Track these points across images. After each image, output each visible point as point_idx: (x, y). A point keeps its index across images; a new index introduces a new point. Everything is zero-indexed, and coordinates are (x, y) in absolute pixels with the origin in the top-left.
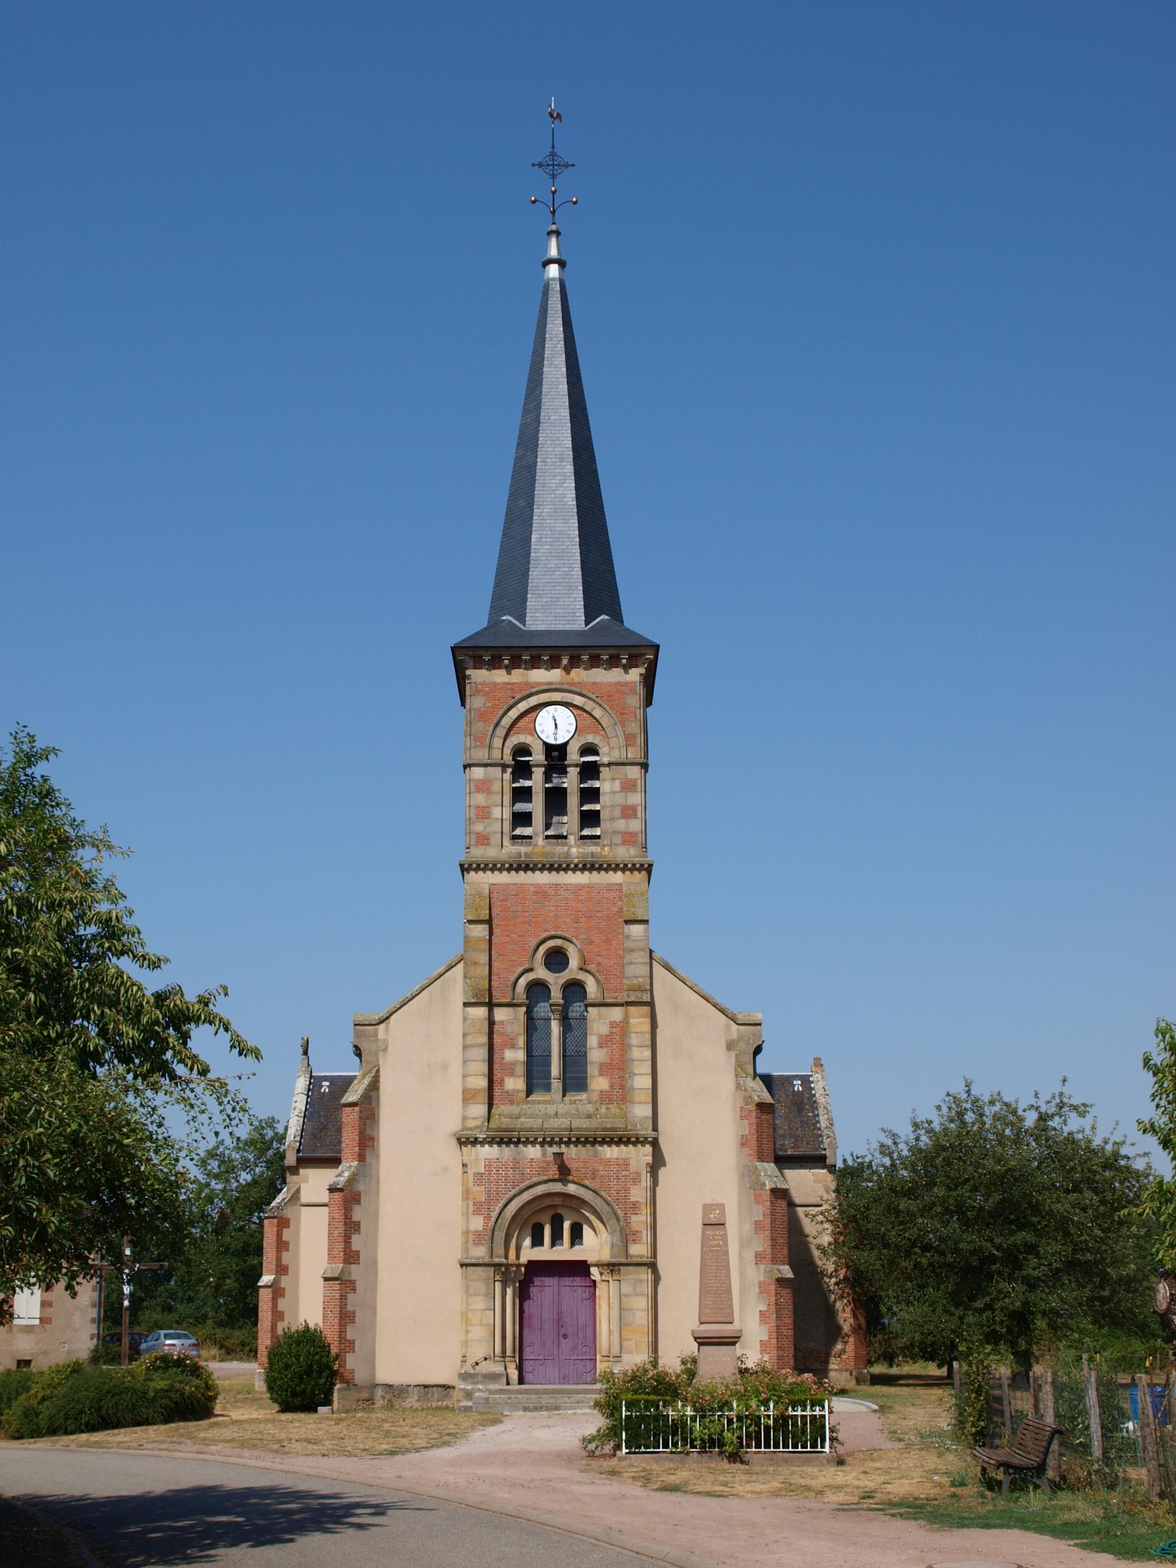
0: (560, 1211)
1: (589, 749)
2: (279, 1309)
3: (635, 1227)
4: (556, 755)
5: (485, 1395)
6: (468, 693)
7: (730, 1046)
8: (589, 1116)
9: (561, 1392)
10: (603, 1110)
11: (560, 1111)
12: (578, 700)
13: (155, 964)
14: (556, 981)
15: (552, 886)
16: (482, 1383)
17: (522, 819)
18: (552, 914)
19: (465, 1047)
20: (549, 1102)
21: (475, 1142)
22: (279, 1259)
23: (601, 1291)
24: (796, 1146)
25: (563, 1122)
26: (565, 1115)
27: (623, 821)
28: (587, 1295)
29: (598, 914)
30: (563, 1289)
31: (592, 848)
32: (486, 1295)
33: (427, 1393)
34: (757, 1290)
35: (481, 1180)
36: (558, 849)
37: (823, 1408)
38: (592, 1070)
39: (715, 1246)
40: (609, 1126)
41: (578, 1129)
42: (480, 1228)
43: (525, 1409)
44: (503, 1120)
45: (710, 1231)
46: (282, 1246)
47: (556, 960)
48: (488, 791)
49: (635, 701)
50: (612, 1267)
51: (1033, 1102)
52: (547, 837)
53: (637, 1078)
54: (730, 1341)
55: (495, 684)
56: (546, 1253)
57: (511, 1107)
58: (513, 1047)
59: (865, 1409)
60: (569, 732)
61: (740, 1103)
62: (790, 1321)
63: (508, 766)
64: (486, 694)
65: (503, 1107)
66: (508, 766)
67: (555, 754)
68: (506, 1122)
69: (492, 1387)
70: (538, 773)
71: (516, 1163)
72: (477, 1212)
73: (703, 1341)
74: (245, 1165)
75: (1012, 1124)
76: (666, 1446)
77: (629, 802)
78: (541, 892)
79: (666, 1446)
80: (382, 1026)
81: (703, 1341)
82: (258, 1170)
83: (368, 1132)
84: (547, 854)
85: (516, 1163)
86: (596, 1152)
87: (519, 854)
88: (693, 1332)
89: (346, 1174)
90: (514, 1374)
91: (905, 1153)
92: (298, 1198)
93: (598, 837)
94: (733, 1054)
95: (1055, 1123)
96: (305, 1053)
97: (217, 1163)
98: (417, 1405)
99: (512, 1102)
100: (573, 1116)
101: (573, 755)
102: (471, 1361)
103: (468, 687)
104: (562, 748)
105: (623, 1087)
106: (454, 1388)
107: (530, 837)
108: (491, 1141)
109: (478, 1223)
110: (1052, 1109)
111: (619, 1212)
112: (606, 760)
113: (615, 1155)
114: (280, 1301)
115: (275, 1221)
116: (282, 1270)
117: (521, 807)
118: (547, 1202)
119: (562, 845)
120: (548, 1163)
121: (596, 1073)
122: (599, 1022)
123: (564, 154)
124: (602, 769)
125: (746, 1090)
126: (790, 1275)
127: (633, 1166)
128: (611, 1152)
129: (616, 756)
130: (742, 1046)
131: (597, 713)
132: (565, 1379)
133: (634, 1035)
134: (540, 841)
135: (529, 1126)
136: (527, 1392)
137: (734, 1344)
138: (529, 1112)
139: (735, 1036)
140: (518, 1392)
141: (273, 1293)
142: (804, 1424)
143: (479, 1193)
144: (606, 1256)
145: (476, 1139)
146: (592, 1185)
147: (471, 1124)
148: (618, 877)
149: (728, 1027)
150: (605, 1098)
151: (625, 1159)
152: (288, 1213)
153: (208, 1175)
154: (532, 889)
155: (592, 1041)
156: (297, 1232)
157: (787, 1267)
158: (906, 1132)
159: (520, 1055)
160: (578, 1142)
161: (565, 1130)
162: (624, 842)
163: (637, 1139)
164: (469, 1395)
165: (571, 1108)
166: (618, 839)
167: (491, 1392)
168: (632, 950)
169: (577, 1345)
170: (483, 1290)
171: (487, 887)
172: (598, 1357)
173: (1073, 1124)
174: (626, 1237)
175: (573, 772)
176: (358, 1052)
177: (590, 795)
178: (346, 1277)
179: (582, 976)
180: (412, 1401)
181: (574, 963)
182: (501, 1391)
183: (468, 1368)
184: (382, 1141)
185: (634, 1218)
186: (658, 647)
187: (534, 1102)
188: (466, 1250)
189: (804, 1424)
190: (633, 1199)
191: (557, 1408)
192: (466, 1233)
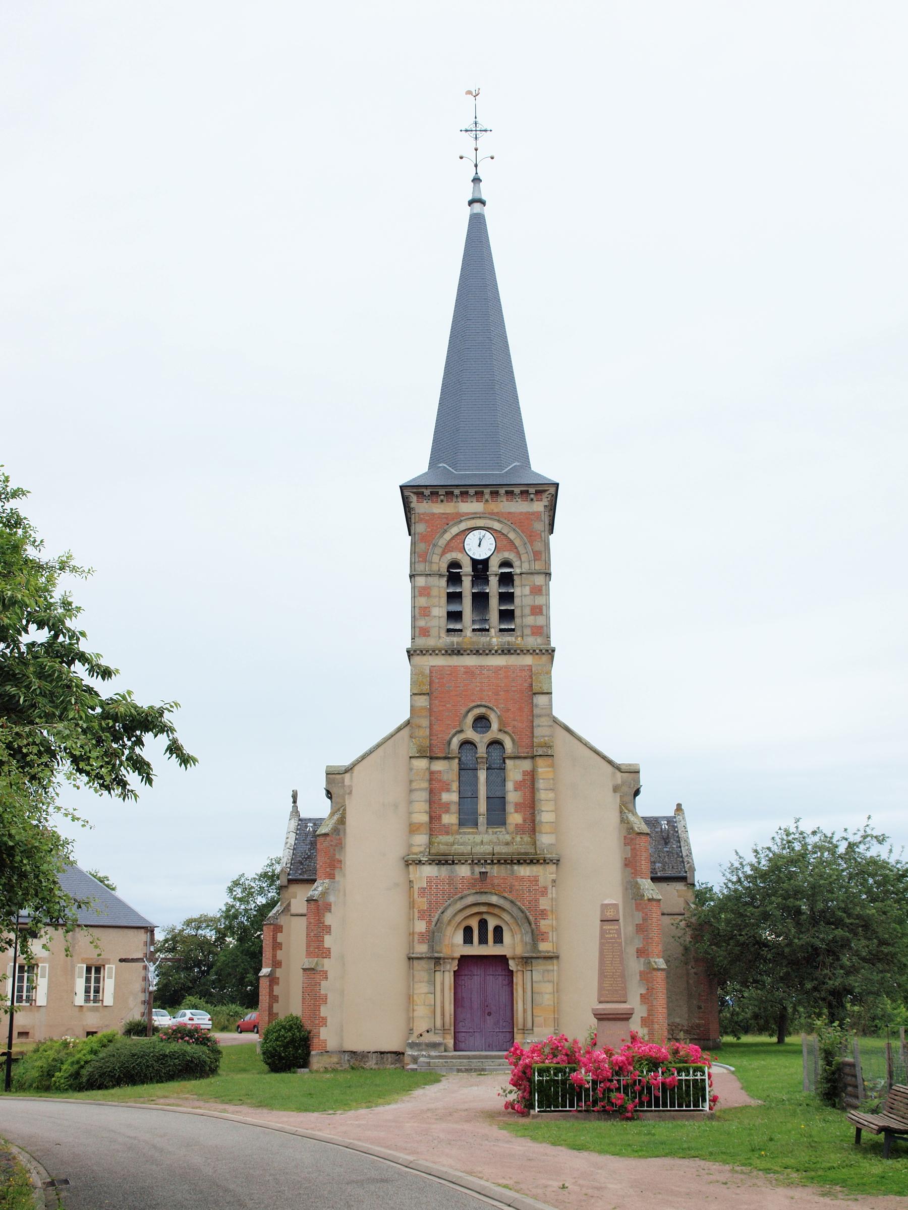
0: (485, 917)
1: (506, 564)
2: (275, 993)
4: (480, 567)
5: (427, 1060)
6: (413, 521)
7: (616, 789)
8: (507, 844)
9: (486, 1057)
10: (518, 839)
11: (485, 840)
12: (497, 526)
13: (106, 673)
14: (481, 740)
15: (477, 667)
17: (455, 616)
18: (478, 689)
19: (411, 791)
20: (476, 833)
22: (274, 956)
23: (518, 979)
24: (664, 869)
25: (487, 849)
27: (532, 617)
28: (505, 982)
29: (513, 689)
30: (488, 977)
31: (508, 638)
32: (429, 982)
33: (382, 1058)
34: (638, 977)
35: (424, 893)
36: (483, 639)
37: (704, 1073)
38: (510, 808)
39: (611, 938)
40: (523, 851)
41: (499, 854)
42: (424, 930)
43: (459, 1071)
44: (441, 847)
45: (607, 927)
46: (277, 946)
47: (482, 722)
48: (428, 595)
49: (539, 526)
50: (526, 961)
51: (844, 835)
52: (474, 630)
53: (544, 814)
54: (625, 1017)
55: (433, 514)
56: (476, 949)
57: (448, 837)
58: (448, 790)
59: (725, 1071)
60: (490, 550)
61: (624, 833)
62: (664, 1001)
63: (443, 576)
64: (427, 521)
66: (443, 576)
67: (480, 566)
68: (443, 848)
70: (467, 581)
71: (451, 880)
72: (421, 918)
73: (602, 1017)
74: (261, 891)
75: (829, 850)
76: (572, 1106)
77: (537, 603)
78: (469, 672)
79: (572, 1106)
80: (347, 776)
81: (602, 1017)
82: (270, 895)
83: (337, 857)
84: (473, 642)
85: (451, 880)
87: (453, 643)
88: (593, 1010)
89: (320, 889)
90: (450, 1042)
91: (750, 872)
92: (289, 910)
93: (513, 630)
94: (618, 795)
95: (861, 848)
96: (295, 802)
97: (240, 890)
98: (374, 1067)
99: (447, 833)
101: (494, 567)
102: (416, 1033)
103: (413, 516)
104: (485, 562)
105: (533, 821)
106: (403, 1054)
107: (461, 631)
108: (431, 862)
109: (421, 926)
110: (857, 839)
111: (531, 918)
112: (518, 571)
113: (528, 874)
114: (275, 987)
115: (272, 927)
116: (276, 964)
117: (454, 608)
119: (485, 636)
120: (475, 880)
121: (513, 810)
122: (515, 771)
123: (483, 124)
124: (515, 577)
125: (628, 823)
126: (664, 966)
127: (542, 882)
128: (524, 871)
129: (526, 567)
130: (625, 789)
131: (512, 536)
132: (490, 1048)
133: (541, 781)
134: (468, 633)
135: (460, 851)
136: (460, 1057)
137: (627, 1019)
138: (461, 841)
139: (619, 782)
140: (453, 1057)
141: (270, 981)
142: (688, 1087)
143: (422, 903)
144: (519, 951)
145: (420, 861)
146: (510, 897)
147: (416, 849)
148: (528, 660)
149: (614, 775)
150: (519, 829)
151: (535, 877)
152: (282, 921)
153: (234, 899)
154: (462, 669)
155: (510, 786)
157: (661, 960)
158: (751, 858)
159: (454, 797)
161: (489, 854)
162: (533, 634)
163: (545, 861)
164: (415, 1060)
165: (494, 838)
166: (527, 631)
168: (540, 716)
169: (498, 1021)
171: (428, 668)
173: (875, 851)
174: (536, 936)
175: (494, 581)
176: (329, 794)
177: (506, 598)
178: (319, 968)
179: (501, 736)
180: (371, 1063)
181: (495, 726)
182: (440, 1057)
183: (413, 1039)
184: (348, 863)
185: (543, 922)
186: (558, 484)
187: (465, 833)
188: (411, 946)
189: (688, 1087)
190: (542, 907)
191: (483, 1070)
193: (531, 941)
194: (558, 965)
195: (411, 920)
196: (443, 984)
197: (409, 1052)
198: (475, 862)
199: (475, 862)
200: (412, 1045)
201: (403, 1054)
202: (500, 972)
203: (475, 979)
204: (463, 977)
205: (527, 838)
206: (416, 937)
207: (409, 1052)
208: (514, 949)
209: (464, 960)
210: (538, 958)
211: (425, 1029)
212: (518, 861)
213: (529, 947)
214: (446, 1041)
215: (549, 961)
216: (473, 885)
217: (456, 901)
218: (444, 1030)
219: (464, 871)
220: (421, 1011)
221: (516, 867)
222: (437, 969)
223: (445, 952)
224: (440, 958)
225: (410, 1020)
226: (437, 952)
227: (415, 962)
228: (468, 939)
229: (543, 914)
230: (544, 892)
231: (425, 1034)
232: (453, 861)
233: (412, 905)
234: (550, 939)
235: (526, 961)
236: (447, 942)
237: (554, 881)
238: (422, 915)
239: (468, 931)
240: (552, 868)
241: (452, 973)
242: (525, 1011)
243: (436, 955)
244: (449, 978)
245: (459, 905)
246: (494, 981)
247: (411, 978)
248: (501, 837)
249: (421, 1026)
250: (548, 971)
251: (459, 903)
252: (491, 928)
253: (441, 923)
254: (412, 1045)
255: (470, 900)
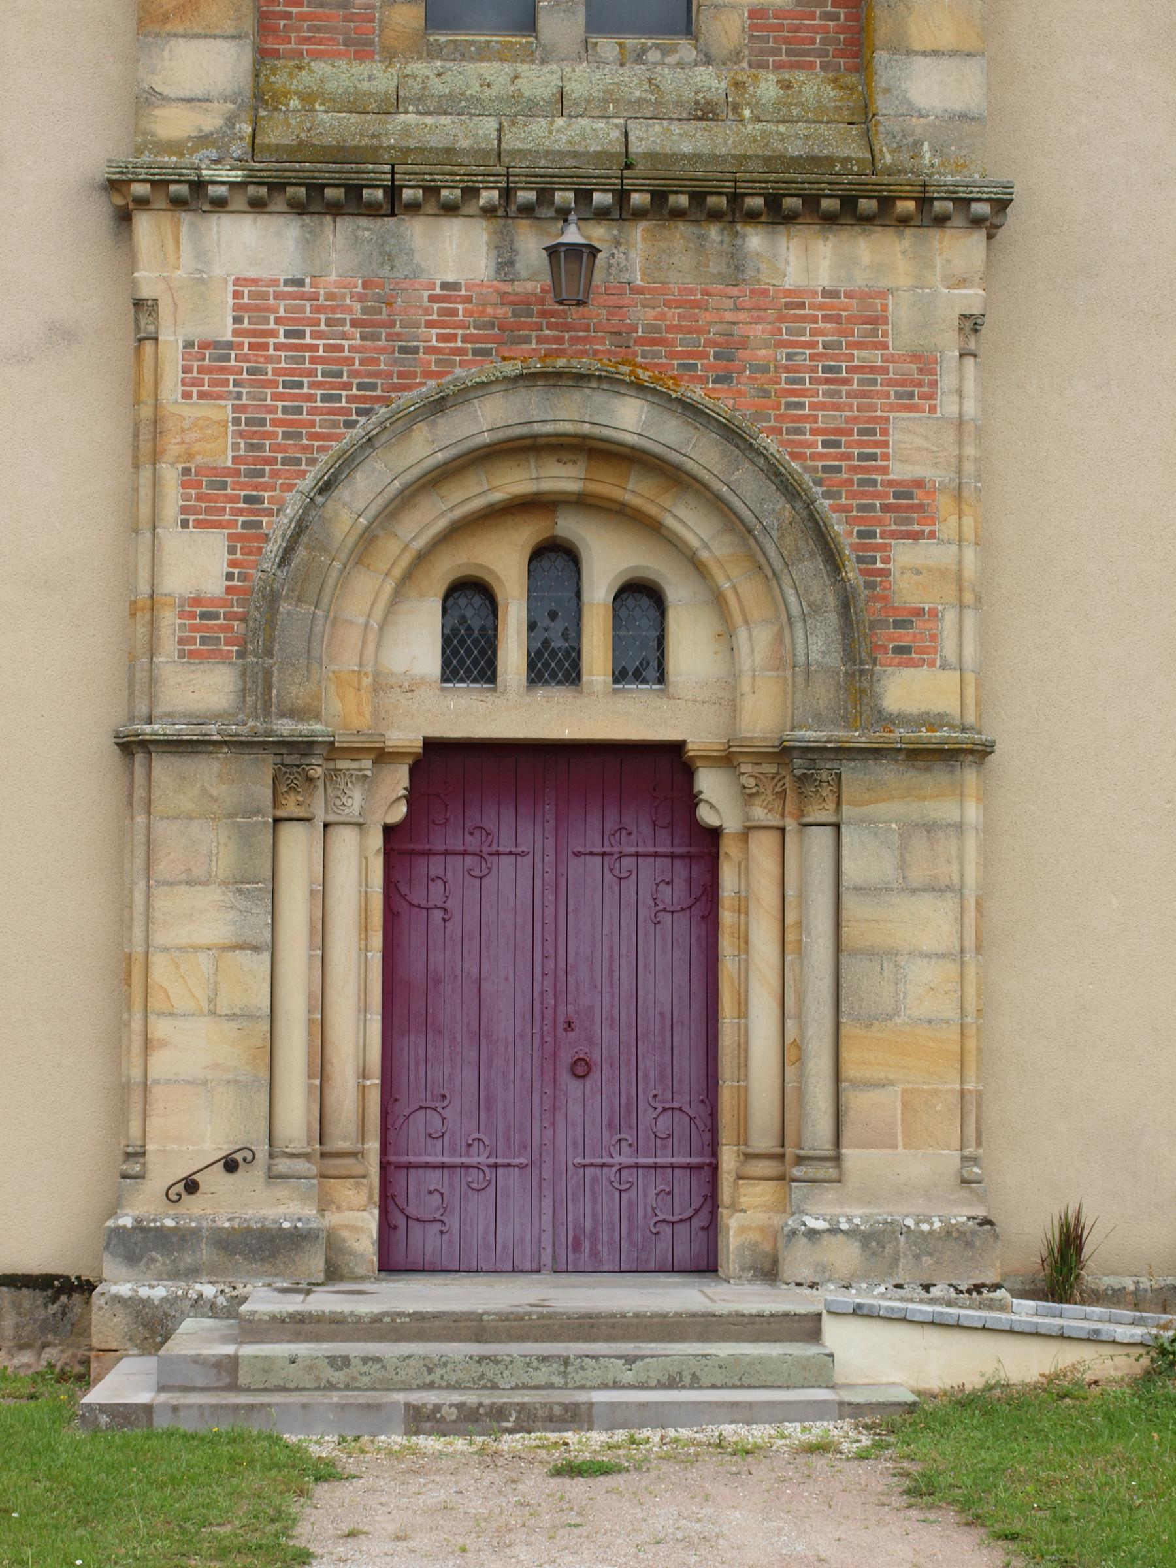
0: (569, 526)
3: (907, 591)
8: (705, 112)
9: (588, 1326)
16: (214, 1272)
20: (528, 56)
21: (194, 197)
23: (749, 879)
25: (596, 134)
26: (599, 107)
28: (676, 894)
30: (576, 865)
32: (239, 883)
42: (214, 585)
43: (420, 1420)
50: (802, 771)
56: (512, 711)
63: (247, 36)
65: (321, 68)
68: (332, 126)
69: (263, 1300)
71: (379, 310)
85: (379, 310)
86: (737, 264)
90: (358, 1224)
100: (637, 111)
102: (164, 1171)
106: (87, 1287)
109: (198, 564)
113: (824, 278)
118: (514, 481)
120: (521, 305)
127: (902, 330)
128: (803, 262)
136: (423, 1326)
138: (438, 87)
143: (206, 429)
144: (762, 717)
145: (199, 186)
146: (723, 403)
147: (175, 124)
151: (865, 296)
156: (627, 1309)
160: (660, 208)
161: (601, 157)
163: (924, 202)
167: (254, 1329)
170: (225, 861)
172: (728, 1159)
174: (868, 630)
182: (300, 1326)
183: (145, 1206)
185: (904, 555)
187: (461, 54)
188: (139, 671)
190: (900, 471)
192: (145, 608)
193: (834, 659)
194: (984, 798)
195: (140, 526)
196: (322, 894)
197: (120, 1284)
198: (515, 194)
199: (515, 194)
200: (140, 1245)
201: (87, 1287)
202: (642, 834)
203: (510, 872)
204: (436, 866)
205: (814, 87)
206: (169, 620)
207: (120, 1284)
208: (734, 708)
209: (445, 768)
210: (876, 753)
211: (214, 1147)
212: (773, 202)
213: (823, 695)
214: (333, 1219)
215: (940, 776)
216: (508, 334)
217: (404, 424)
218: (325, 1152)
219: (454, 253)
220: (192, 1049)
221: (755, 240)
222: (291, 807)
223: (342, 714)
224: (304, 747)
225: (128, 1097)
226: (293, 713)
227: (163, 768)
228: (468, 656)
229: (909, 506)
230: (916, 386)
231: (215, 1181)
232: (393, 192)
233: (146, 439)
234: (948, 647)
235: (802, 771)
236: (347, 661)
237: (972, 324)
238: (204, 504)
239: (470, 597)
240: (960, 249)
241: (376, 840)
242: (790, 1053)
243: (286, 728)
244: (356, 869)
245: (424, 448)
246: (609, 889)
247: (133, 866)
248: (668, 78)
249: (191, 1130)
250: (930, 828)
251: (421, 432)
252: (598, 591)
253: (321, 546)
254: (140, 1245)
255: (489, 418)
